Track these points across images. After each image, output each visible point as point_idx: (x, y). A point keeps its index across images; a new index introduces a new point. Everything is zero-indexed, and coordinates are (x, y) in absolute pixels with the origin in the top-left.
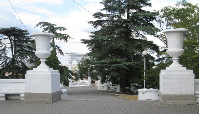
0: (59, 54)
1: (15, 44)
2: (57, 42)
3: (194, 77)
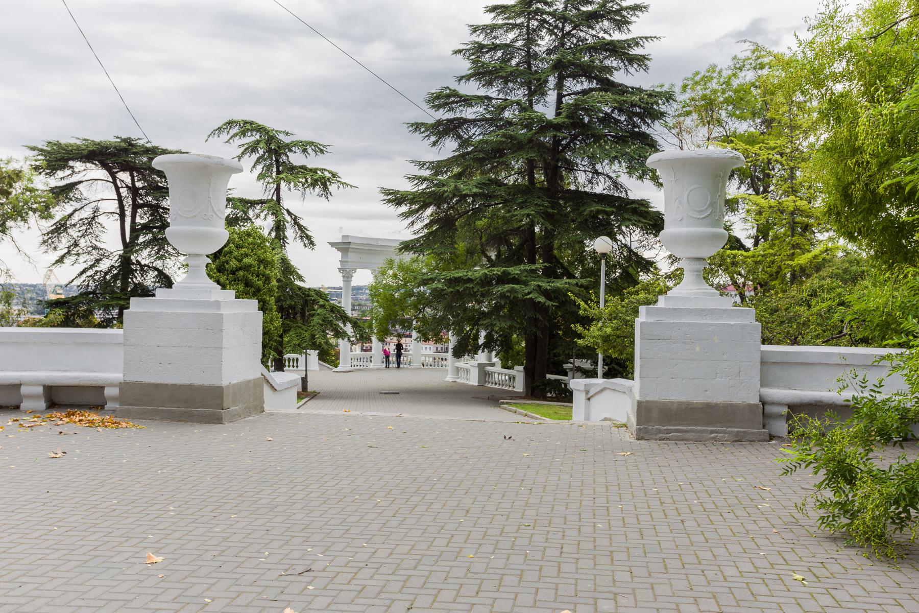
0: (299, 244)
1: (134, 200)
2: (295, 200)
3: (758, 337)
